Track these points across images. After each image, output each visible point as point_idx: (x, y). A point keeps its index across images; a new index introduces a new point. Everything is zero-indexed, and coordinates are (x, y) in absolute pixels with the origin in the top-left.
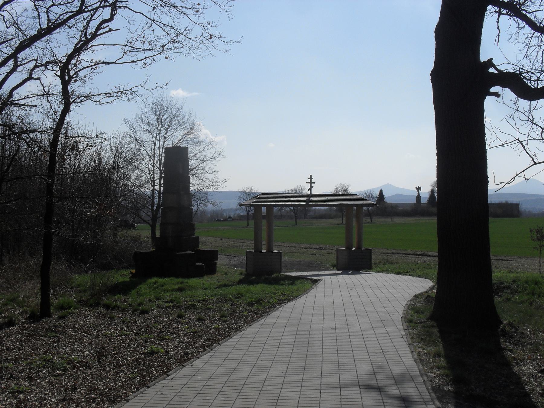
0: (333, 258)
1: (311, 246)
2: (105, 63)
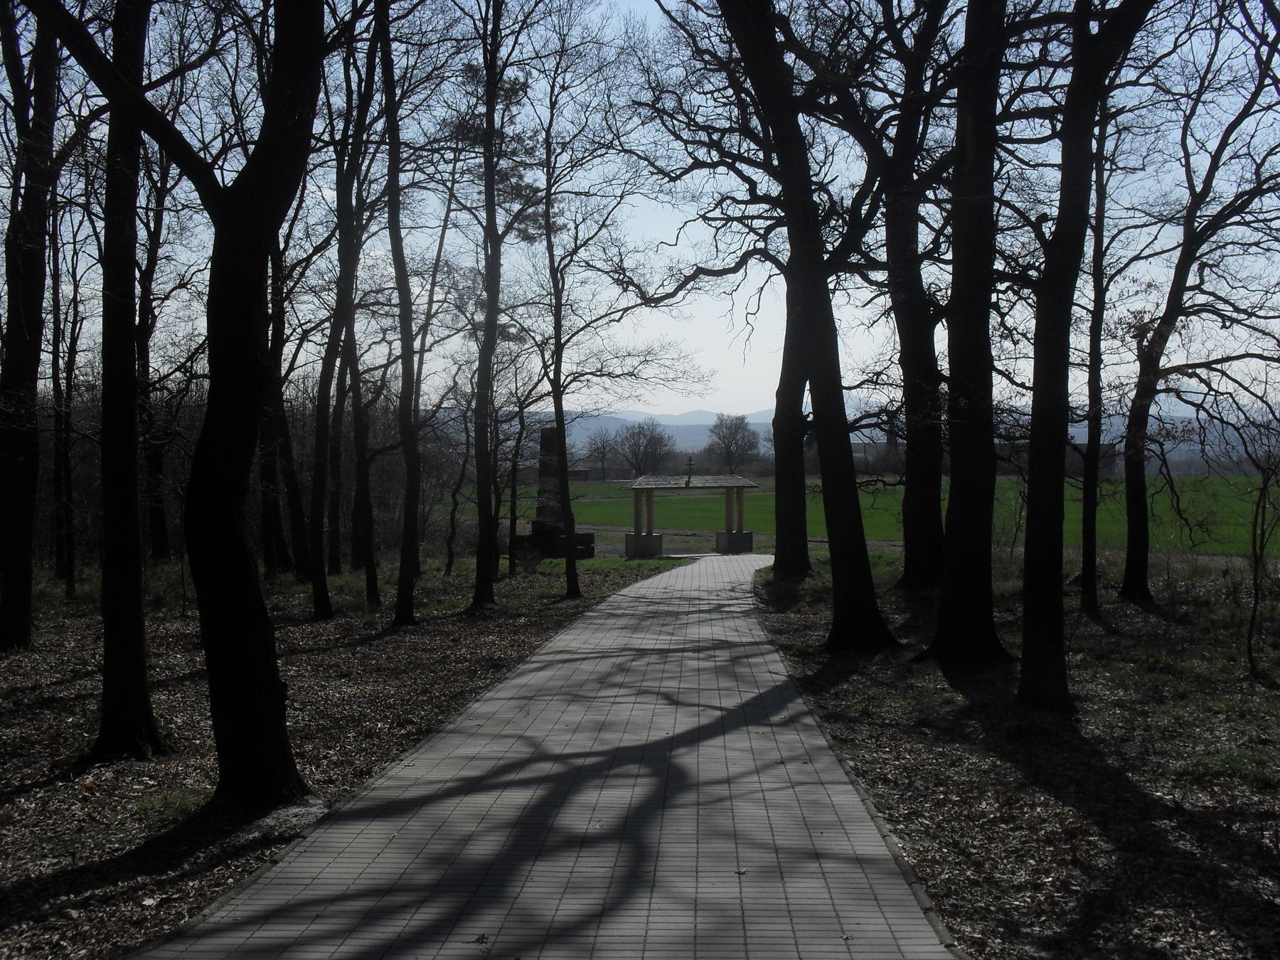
0: (713, 544)
1: (681, 532)
2: (1264, 333)
